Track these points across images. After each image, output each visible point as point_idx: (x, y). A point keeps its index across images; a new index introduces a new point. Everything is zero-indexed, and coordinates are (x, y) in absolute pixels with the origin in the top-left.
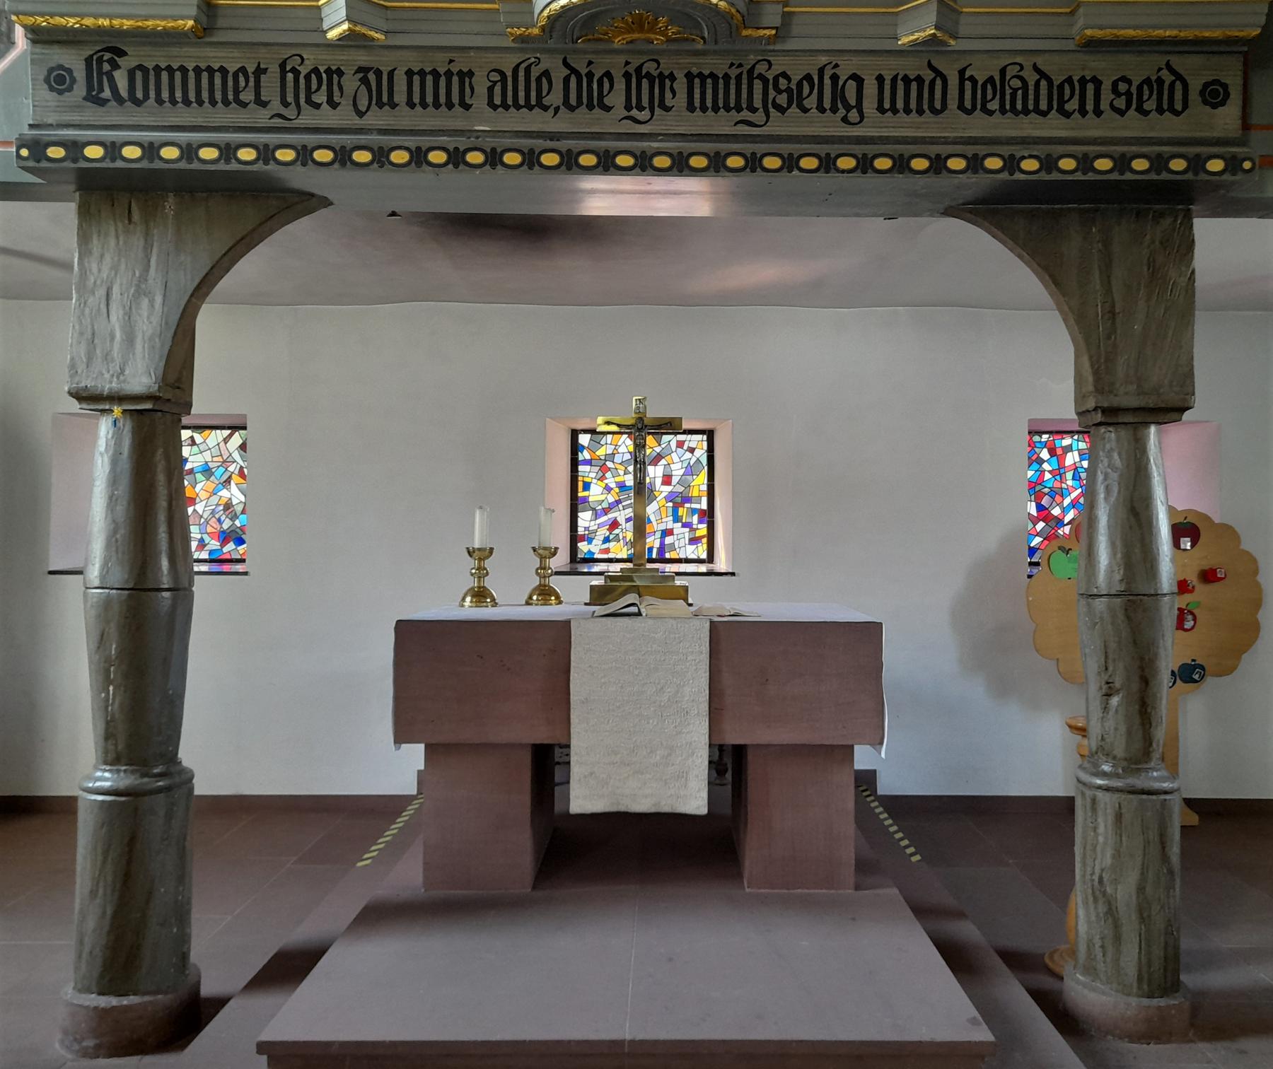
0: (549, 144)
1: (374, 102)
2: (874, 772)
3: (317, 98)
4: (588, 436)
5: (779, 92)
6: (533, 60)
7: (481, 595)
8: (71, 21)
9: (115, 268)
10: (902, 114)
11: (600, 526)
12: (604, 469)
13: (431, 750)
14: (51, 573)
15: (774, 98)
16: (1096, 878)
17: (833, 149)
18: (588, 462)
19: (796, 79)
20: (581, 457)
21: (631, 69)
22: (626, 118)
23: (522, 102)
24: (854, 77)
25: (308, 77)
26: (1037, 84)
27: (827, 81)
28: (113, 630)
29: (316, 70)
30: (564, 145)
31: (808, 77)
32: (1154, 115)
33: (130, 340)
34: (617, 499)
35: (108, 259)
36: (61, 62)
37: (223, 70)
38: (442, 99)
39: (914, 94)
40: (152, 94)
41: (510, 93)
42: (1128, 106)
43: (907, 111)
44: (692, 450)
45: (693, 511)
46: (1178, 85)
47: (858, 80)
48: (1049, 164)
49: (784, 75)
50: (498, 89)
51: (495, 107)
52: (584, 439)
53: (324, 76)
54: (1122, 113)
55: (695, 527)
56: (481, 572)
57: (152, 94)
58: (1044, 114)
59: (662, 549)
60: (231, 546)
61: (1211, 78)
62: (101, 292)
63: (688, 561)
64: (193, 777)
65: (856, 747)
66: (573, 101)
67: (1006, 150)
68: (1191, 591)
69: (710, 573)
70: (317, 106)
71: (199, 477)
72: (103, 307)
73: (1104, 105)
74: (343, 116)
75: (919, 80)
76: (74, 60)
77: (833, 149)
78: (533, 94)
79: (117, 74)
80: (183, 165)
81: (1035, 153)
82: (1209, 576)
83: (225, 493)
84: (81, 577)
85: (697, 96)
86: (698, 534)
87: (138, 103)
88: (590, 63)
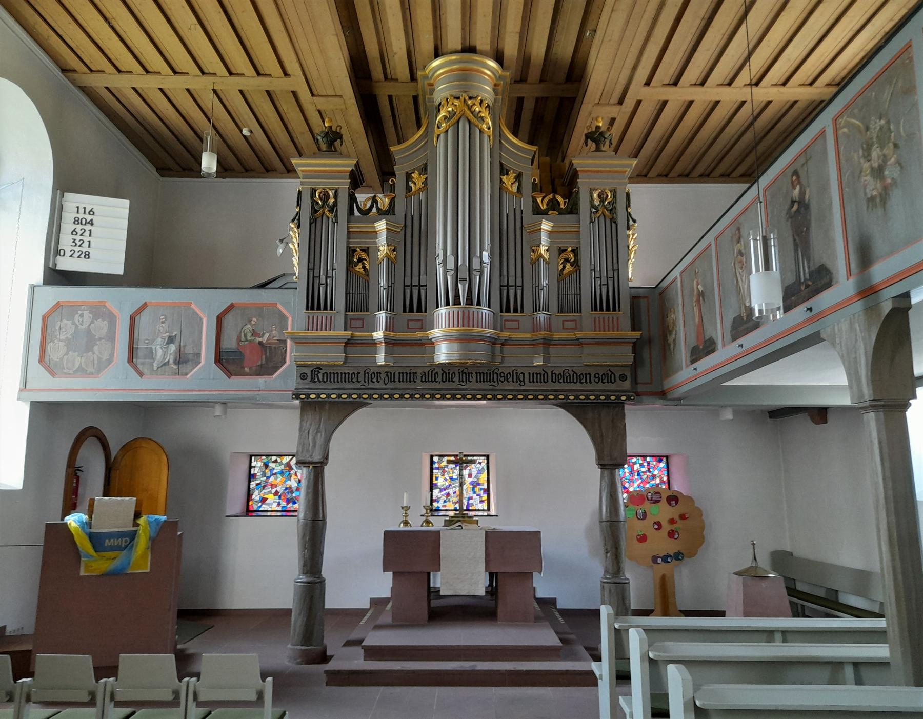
0: (438, 392)
2: (555, 598)
7: (406, 523)
9: (311, 425)
11: (442, 495)
12: (444, 471)
13: (395, 575)
14: (227, 516)
17: (517, 393)
20: (436, 465)
24: (522, 373)
26: (573, 375)
27: (515, 375)
28: (308, 533)
30: (442, 392)
31: (509, 373)
33: (314, 446)
35: (309, 422)
37: (348, 373)
38: (408, 380)
40: (329, 380)
43: (537, 382)
44: (480, 463)
45: (481, 489)
46: (613, 375)
47: (524, 374)
48: (577, 397)
50: (424, 377)
52: (436, 459)
54: (597, 383)
57: (329, 380)
59: (468, 505)
60: (291, 505)
62: (307, 431)
63: (479, 510)
64: (324, 581)
65: (534, 573)
66: (444, 380)
67: (565, 394)
68: (676, 523)
69: (488, 515)
70: (374, 382)
73: (592, 381)
74: (381, 385)
76: (308, 371)
77: (517, 393)
82: (683, 517)
83: (288, 482)
84: (296, 518)
86: (483, 499)
87: (325, 382)
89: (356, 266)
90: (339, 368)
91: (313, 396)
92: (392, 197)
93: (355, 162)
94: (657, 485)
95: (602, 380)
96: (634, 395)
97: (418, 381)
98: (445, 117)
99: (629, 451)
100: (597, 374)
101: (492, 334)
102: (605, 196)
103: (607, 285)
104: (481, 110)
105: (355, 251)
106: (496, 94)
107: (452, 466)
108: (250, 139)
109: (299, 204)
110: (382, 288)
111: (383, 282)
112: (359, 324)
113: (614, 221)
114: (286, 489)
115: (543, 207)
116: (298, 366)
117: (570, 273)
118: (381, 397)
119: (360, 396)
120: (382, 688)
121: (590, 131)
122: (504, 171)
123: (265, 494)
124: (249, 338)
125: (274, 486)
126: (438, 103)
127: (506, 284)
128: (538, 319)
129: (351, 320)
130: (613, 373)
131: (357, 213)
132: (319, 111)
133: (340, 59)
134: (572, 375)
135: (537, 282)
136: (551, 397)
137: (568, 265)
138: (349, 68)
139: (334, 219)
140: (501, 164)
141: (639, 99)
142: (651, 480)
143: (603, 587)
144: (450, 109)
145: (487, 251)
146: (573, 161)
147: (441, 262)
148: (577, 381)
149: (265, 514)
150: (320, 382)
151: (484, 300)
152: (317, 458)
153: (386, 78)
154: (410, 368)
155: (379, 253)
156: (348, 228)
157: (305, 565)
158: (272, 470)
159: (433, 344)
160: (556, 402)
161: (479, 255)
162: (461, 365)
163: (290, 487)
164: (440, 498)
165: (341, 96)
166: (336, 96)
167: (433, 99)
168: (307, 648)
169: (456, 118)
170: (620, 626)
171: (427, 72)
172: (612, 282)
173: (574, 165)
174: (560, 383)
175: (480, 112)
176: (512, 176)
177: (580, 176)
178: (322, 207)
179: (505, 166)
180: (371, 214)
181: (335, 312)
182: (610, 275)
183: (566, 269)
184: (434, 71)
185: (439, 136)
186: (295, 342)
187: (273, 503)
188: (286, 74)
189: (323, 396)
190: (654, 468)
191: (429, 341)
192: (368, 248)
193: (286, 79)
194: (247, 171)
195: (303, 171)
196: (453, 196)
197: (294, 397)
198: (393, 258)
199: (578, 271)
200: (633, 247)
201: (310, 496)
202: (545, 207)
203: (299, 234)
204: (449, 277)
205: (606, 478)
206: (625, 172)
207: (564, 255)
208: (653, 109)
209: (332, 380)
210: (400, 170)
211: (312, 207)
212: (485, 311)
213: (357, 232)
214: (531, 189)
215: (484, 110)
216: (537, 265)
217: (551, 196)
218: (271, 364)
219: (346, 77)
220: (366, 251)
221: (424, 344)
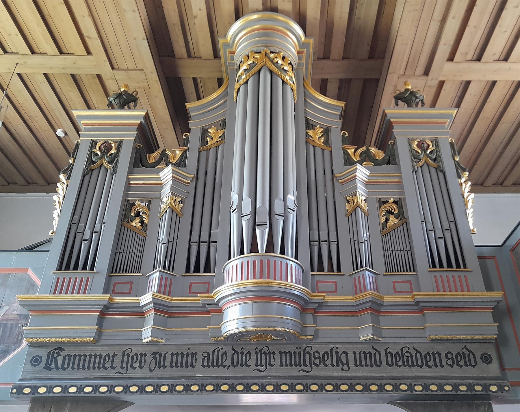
0: (225, 381)
17: (339, 382)
19: (322, 353)
21: (258, 350)
24: (344, 352)
25: (133, 357)
27: (334, 354)
29: (136, 354)
30: (231, 381)
31: (326, 353)
32: (464, 367)
37: (100, 355)
38: (184, 364)
40: (71, 366)
41: (211, 361)
43: (367, 365)
47: (347, 354)
48: (426, 388)
49: (317, 352)
50: (206, 359)
51: (204, 367)
54: (452, 366)
57: (71, 366)
58: (421, 367)
66: (235, 363)
67: (408, 382)
70: (135, 368)
73: (444, 363)
74: (145, 372)
76: (43, 353)
77: (339, 382)
88: (242, 348)
90: (89, 348)
92: (186, 149)
96: (509, 384)
98: (245, 70)
102: (426, 145)
108: (63, 140)
111: (163, 237)
112: (126, 288)
113: (440, 170)
117: (395, 227)
122: (309, 125)
127: (317, 239)
129: (115, 283)
130: (470, 352)
133: (134, 11)
140: (307, 120)
141: (442, 79)
146: (386, 111)
148: (423, 364)
150: (57, 368)
153: (189, 56)
155: (162, 206)
162: (261, 335)
165: (142, 70)
169: (257, 68)
171: (229, 39)
172: (450, 234)
173: (388, 116)
174: (400, 366)
176: (320, 131)
177: (395, 127)
178: (101, 158)
179: (311, 122)
182: (446, 226)
183: (390, 221)
191: (215, 307)
193: (89, 57)
195: (85, 125)
197: (14, 391)
199: (405, 225)
206: (445, 123)
207: (385, 207)
208: (454, 96)
209: (76, 366)
210: (195, 126)
212: (291, 263)
214: (341, 143)
217: (364, 149)
219: (144, 39)
221: (208, 313)
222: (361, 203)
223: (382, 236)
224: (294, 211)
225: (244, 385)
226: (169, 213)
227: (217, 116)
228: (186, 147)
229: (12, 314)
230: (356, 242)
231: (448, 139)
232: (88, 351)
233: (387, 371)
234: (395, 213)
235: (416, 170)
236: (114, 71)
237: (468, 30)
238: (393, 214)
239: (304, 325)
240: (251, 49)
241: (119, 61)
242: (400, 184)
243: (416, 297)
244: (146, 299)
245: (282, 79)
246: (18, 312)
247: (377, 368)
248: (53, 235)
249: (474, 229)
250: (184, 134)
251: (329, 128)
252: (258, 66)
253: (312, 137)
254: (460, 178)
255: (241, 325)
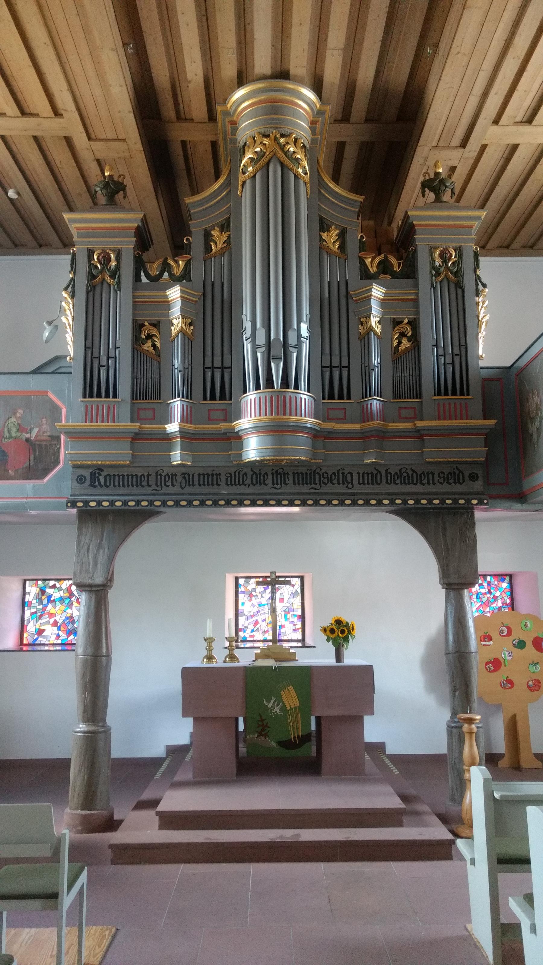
1: (187, 484)
2: (384, 743)
3: (168, 484)
4: (243, 580)
5: (324, 478)
6: (241, 469)
8: (89, 462)
10: (366, 485)
12: (251, 595)
13: (196, 720)
15: (323, 480)
16: (453, 762)
18: (244, 592)
19: (330, 473)
20: (241, 589)
21: (274, 471)
22: (273, 487)
23: (237, 483)
24: (350, 473)
25: (165, 477)
26: (412, 474)
27: (341, 475)
29: (168, 474)
31: (334, 473)
32: (453, 484)
33: (96, 564)
34: (258, 610)
36: (82, 474)
37: (136, 475)
38: (210, 483)
39: (370, 478)
40: (112, 484)
41: (233, 480)
42: (444, 481)
43: (368, 483)
44: (293, 586)
46: (461, 474)
47: (352, 475)
49: (326, 473)
51: (228, 485)
52: (241, 581)
53: (170, 476)
54: (442, 484)
55: (295, 623)
56: (210, 649)
57: (112, 484)
58: (416, 484)
60: (72, 637)
61: (471, 472)
62: (86, 547)
66: (254, 482)
67: (403, 497)
70: (168, 486)
71: (57, 603)
72: (86, 553)
73: (436, 481)
74: (176, 489)
75: (372, 473)
76: (86, 473)
78: (241, 480)
79: (100, 477)
80: (123, 508)
81: (412, 498)
84: (74, 652)
85: (296, 480)
86: (298, 627)
87: (107, 487)
88: (260, 470)
89: (144, 344)
90: (126, 469)
91: (93, 504)
92: (189, 258)
93: (142, 216)
94: (499, 609)
95: (448, 480)
97: (223, 483)
98: (252, 159)
99: (482, 569)
100: (442, 472)
101: (313, 424)
102: (448, 255)
103: (453, 364)
104: (296, 150)
105: (143, 325)
106: (313, 131)
107: (261, 588)
108: (18, 204)
109: (73, 269)
110: (176, 371)
111: (177, 363)
112: (149, 414)
113: (459, 286)
114: (67, 618)
115: (373, 270)
116: (75, 467)
118: (177, 504)
119: (151, 503)
120: (182, 866)
121: (427, 178)
123: (41, 624)
124: (14, 434)
125: (51, 615)
126: (242, 144)
128: (369, 407)
131: (144, 279)
132: (98, 161)
133: (121, 86)
134: (410, 474)
135: (367, 360)
136: (386, 502)
137: (404, 341)
138: (132, 100)
139: (116, 286)
141: (484, 142)
142: (494, 603)
143: (451, 732)
144: (258, 149)
145: (305, 323)
147: (248, 336)
148: (417, 482)
149: (42, 648)
150: (101, 486)
151: (303, 383)
152: (99, 579)
153: (179, 118)
154: (212, 468)
155: (173, 328)
156: (134, 297)
157: (85, 711)
158: (49, 597)
159: (240, 438)
160: (392, 508)
161: (295, 327)
163: (71, 617)
164: (247, 627)
165: (124, 140)
166: (118, 139)
167: (236, 139)
168: (88, 812)
169: (265, 160)
170: (501, 796)
171: (229, 106)
173: (411, 218)
174: (397, 484)
175: (294, 152)
176: (334, 233)
179: (325, 221)
180: (161, 280)
181: (119, 400)
182: (457, 351)
184: (236, 104)
185: (244, 183)
186: (70, 438)
187: (51, 633)
188: (57, 113)
189: (106, 504)
190: (496, 589)
192: (159, 322)
193: (59, 120)
194: (16, 245)
195: (78, 229)
196: (262, 211)
197: (69, 505)
198: (190, 333)
199: (416, 348)
200: (484, 317)
201: (91, 627)
202: (375, 269)
203: (73, 305)
204: (259, 355)
205: (453, 600)
206: (472, 226)
207: (398, 328)
209: (117, 484)
211: (90, 273)
213: (146, 302)
215: (299, 150)
216: (366, 342)
217: (382, 257)
218: (41, 466)
220: (156, 325)
221: (229, 439)
222: (374, 327)
223: (393, 361)
224: (307, 339)
225: (263, 501)
226: (181, 337)
227: (219, 215)
228: (189, 256)
229: (43, 436)
230: (367, 368)
231: (472, 247)
232: (125, 472)
233: (385, 488)
234: (408, 335)
235: (435, 286)
236: (91, 142)
237: (516, 95)
238: (406, 336)
239: (315, 451)
240: (258, 131)
241: (98, 131)
242: (416, 302)
243: (417, 425)
244: (173, 427)
245: (294, 173)
246: (48, 434)
247: (378, 486)
248: (71, 361)
249: (482, 354)
250: (185, 239)
251: (345, 229)
252: (267, 157)
253: (326, 242)
254: (478, 297)
255: (261, 454)
